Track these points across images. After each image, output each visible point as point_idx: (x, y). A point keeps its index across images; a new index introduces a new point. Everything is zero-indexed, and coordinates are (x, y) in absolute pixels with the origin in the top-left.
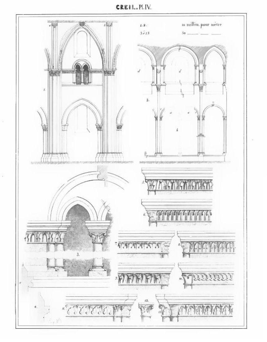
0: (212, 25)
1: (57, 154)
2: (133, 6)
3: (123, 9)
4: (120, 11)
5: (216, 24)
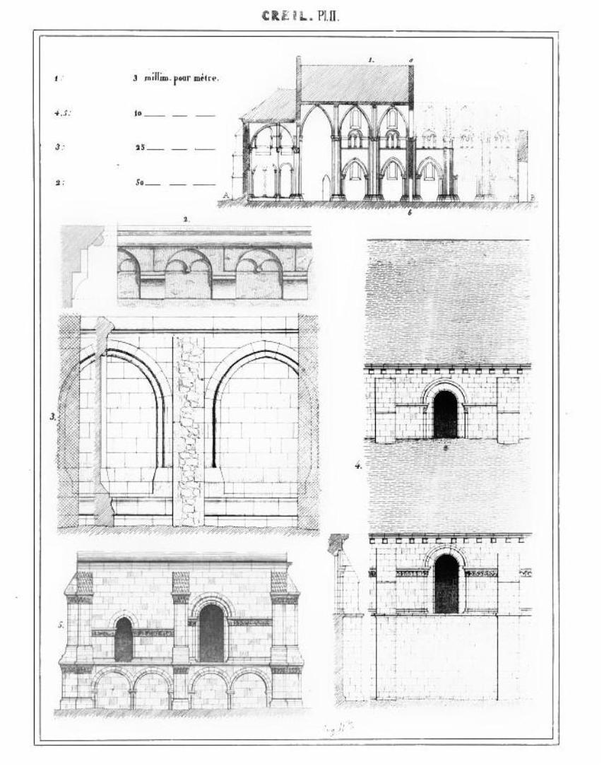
0: (196, 79)
1: (497, 382)
3: (278, 19)
4: (272, 25)
5: (204, 76)
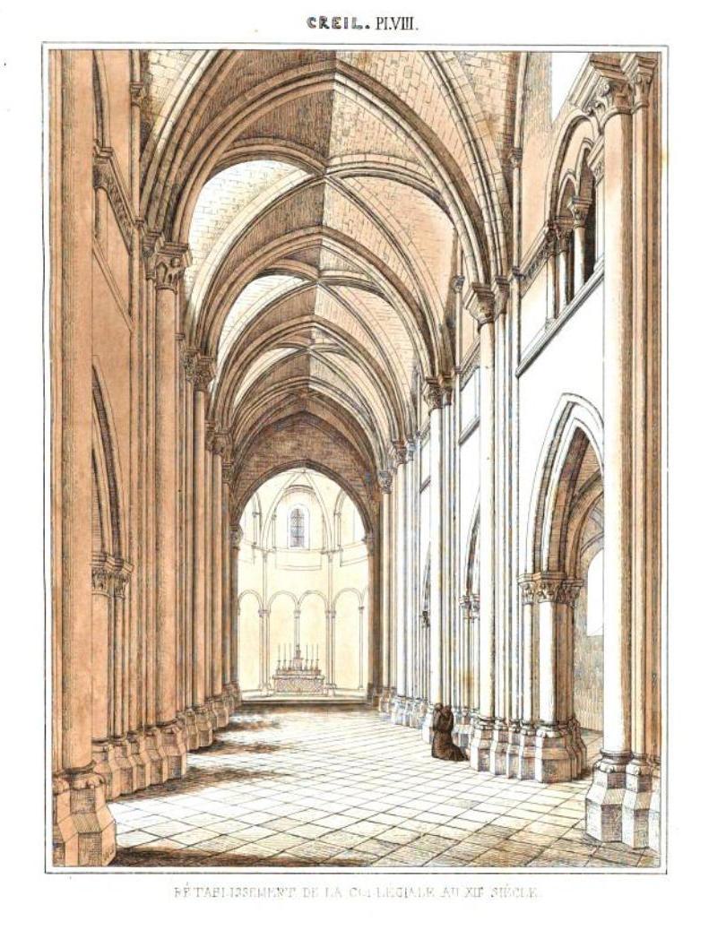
2: (354, 19)
